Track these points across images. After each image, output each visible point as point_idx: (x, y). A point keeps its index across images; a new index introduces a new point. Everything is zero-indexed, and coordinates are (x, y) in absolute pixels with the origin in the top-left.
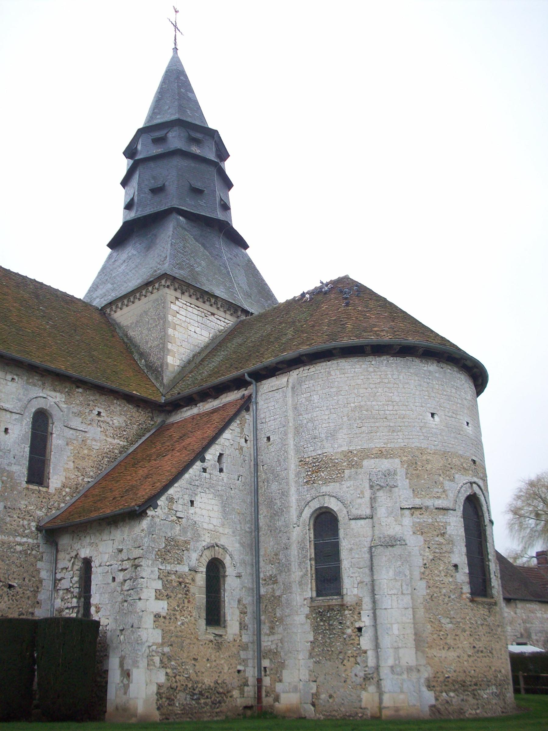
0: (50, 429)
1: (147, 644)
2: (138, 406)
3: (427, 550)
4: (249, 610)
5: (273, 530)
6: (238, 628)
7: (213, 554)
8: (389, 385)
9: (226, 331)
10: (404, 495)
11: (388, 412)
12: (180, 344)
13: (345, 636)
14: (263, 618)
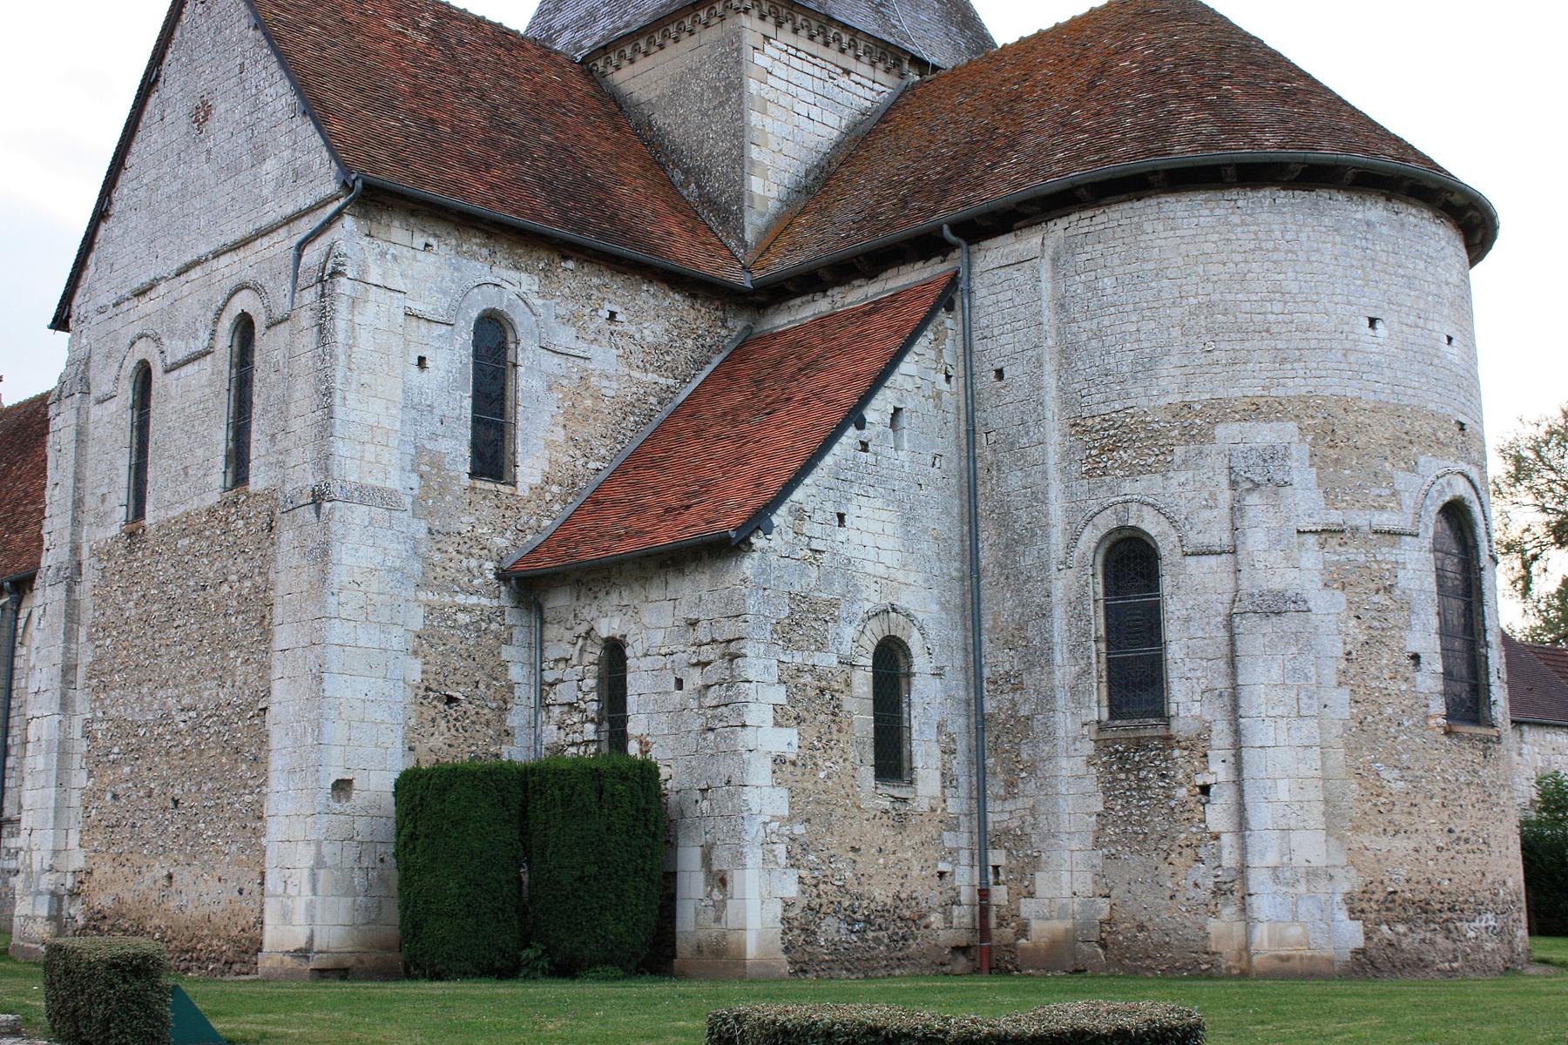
0: (510, 354)
1: (760, 819)
2: (694, 296)
3: (1354, 622)
4: (961, 746)
5: (1014, 577)
6: (939, 784)
7: (885, 627)
8: (1275, 256)
9: (877, 111)
10: (1306, 501)
11: (1271, 318)
12: (777, 148)
13: (1173, 804)
14: (990, 762)
